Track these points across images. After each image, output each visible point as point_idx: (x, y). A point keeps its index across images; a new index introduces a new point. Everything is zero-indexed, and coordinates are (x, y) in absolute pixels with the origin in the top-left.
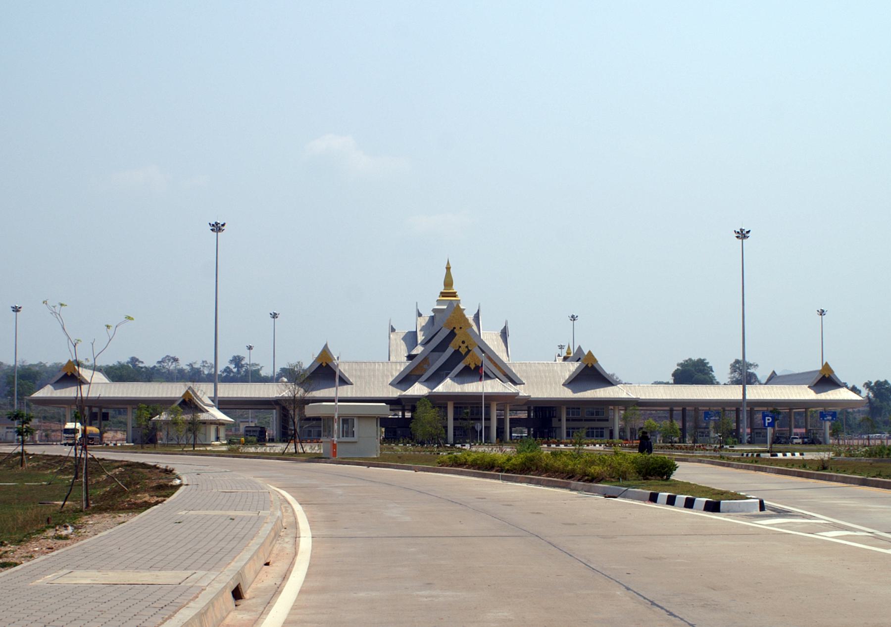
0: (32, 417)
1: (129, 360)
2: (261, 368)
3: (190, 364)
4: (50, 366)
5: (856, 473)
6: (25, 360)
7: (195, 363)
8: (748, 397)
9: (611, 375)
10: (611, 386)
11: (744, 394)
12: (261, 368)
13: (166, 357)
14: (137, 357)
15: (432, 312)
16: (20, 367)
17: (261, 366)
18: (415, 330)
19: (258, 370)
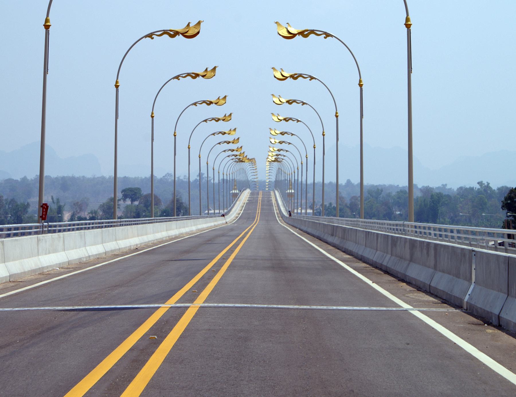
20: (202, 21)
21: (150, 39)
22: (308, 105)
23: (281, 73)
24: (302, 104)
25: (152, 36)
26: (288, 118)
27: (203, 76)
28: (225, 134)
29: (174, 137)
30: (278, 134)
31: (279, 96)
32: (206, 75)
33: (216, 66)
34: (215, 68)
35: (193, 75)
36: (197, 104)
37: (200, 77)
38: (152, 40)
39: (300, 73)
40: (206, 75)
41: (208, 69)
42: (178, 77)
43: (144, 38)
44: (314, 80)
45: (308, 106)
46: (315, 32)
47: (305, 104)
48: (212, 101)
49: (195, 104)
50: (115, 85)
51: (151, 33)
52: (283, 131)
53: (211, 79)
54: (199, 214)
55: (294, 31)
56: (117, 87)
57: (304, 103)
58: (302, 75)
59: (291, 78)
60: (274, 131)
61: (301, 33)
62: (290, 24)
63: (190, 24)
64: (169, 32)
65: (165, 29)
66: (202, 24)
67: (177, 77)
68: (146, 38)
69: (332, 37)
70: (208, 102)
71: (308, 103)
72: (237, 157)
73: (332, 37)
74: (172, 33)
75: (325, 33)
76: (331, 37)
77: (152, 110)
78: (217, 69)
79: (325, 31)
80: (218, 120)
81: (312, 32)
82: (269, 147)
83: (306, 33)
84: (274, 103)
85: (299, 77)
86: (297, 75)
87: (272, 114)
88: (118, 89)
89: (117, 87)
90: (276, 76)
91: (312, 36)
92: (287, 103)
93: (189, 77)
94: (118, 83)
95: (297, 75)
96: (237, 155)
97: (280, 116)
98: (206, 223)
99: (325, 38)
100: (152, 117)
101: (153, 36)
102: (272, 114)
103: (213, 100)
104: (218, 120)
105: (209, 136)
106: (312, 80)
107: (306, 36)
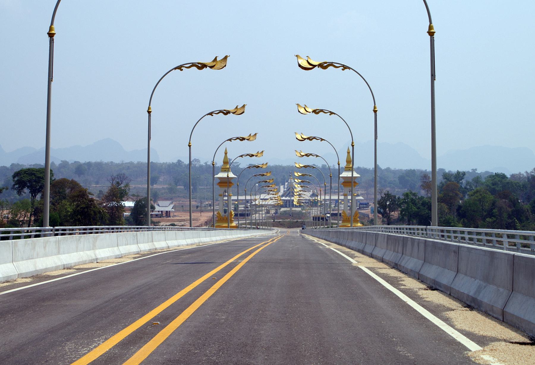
0: (381, 197)
1: (177, 161)
2: (240, 164)
3: (206, 163)
4: (273, 166)
5: (395, 268)
6: (124, 161)
7: (207, 162)
8: (246, 198)
9: (466, 182)
10: (358, 197)
11: (246, 198)
12: (240, 164)
13: (194, 160)
14: (181, 160)
15: (151, 161)
16: (525, 174)
17: (240, 163)
18: (146, 196)
19: (238, 165)
20: (229, 56)
21: (211, 116)
22: (325, 141)
23: (307, 61)
24: (316, 156)
25: (181, 68)
26: (311, 137)
27: (248, 140)
28: (259, 168)
29: (147, 114)
30: (310, 112)
31: (300, 151)
32: (214, 66)
33: (228, 55)
34: (256, 134)
35: (241, 138)
36: (243, 156)
37: (246, 140)
38: (212, 116)
39: (314, 136)
40: (214, 66)
41: (238, 107)
42: (212, 114)
43: (174, 70)
44: (347, 70)
45: (337, 115)
46: (334, 65)
47: (347, 68)
48: (254, 154)
49: (211, 114)
50: (147, 111)
51: (181, 66)
52: (318, 109)
53: (222, 69)
54: (153, 233)
55: (303, 154)
56: (51, 35)
57: (332, 113)
58: (333, 64)
59: (308, 140)
60: (304, 109)
61: (308, 138)
62: (310, 58)
63: (217, 58)
64: (197, 64)
65: (220, 110)
66: (246, 106)
67: (180, 68)
68: (176, 70)
69: (350, 69)
70: (251, 155)
71: (336, 113)
72: (275, 198)
73: (350, 69)
74: (225, 112)
75: (343, 66)
76: (349, 69)
77: (189, 140)
78: (228, 58)
79: (343, 64)
80: (227, 113)
81: (322, 111)
82: (295, 163)
83: (317, 111)
84: (300, 113)
85: (320, 112)
86: (312, 138)
87: (295, 151)
88: (150, 115)
89: (149, 112)
90: (298, 138)
91: (321, 113)
92: (314, 113)
93: (238, 140)
94: (151, 109)
95: (328, 64)
96: (275, 197)
97: (309, 108)
98: (112, 264)
99: (321, 141)
100: (190, 146)
101: (232, 140)
102: (295, 151)
103: (246, 136)
104: (227, 113)
105: (225, 141)
106: (323, 141)
107: (325, 68)
